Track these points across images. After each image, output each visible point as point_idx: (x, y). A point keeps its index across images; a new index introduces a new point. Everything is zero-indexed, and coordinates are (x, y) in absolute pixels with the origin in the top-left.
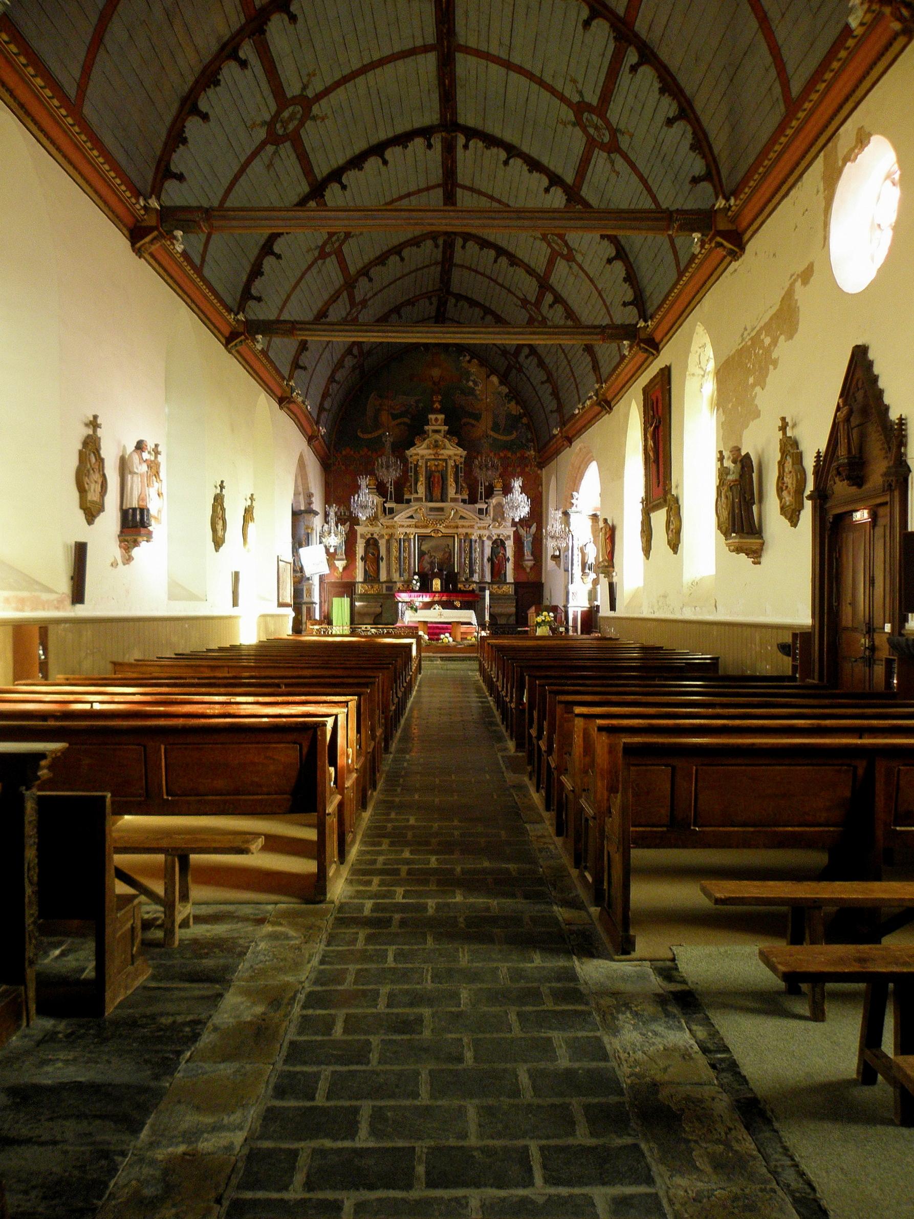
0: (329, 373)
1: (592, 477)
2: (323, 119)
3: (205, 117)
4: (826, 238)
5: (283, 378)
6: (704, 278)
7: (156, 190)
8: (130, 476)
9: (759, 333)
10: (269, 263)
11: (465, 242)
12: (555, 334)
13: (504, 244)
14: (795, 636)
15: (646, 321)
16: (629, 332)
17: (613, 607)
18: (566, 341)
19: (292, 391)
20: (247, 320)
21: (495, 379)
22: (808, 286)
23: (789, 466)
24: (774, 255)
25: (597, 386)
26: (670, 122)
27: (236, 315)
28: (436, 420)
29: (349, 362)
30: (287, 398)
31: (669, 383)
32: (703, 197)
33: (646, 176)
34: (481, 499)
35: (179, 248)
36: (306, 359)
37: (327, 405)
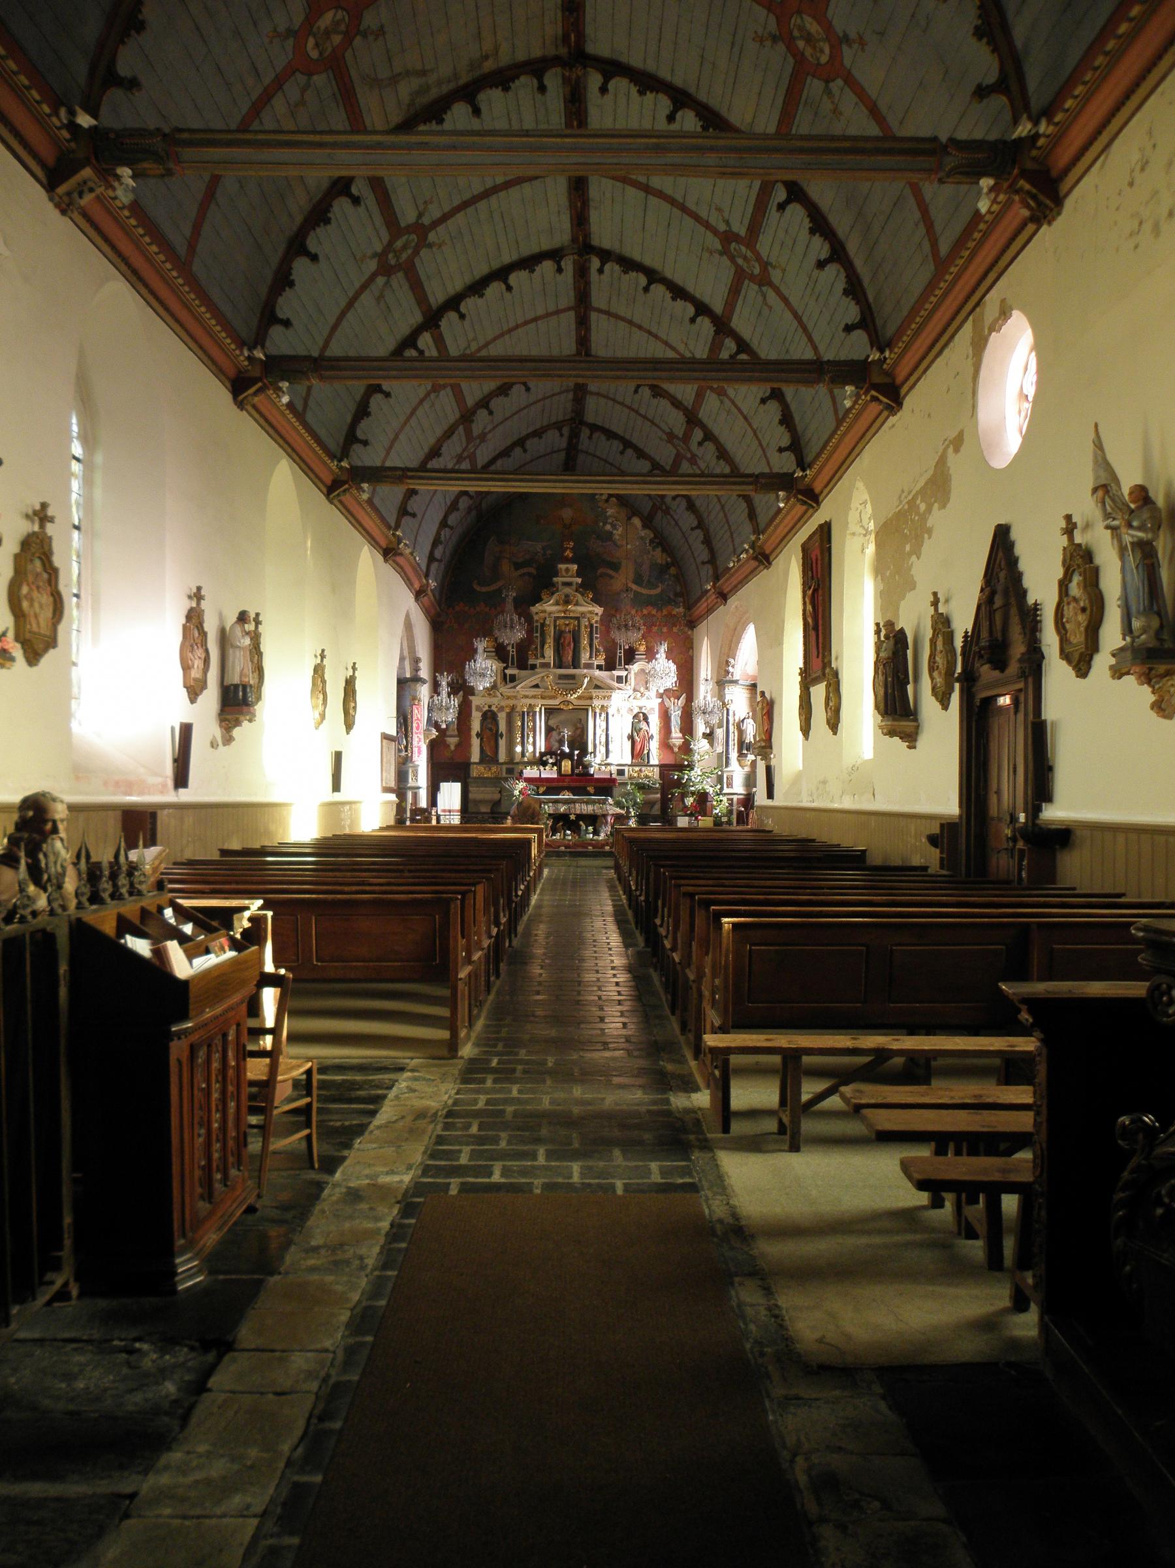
1: (749, 641)
2: (440, 246)
3: (314, 258)
4: (974, 407)
5: (389, 527)
6: (863, 430)
8: (231, 651)
9: (914, 498)
12: (704, 483)
14: (942, 825)
15: (804, 470)
16: (785, 482)
17: (770, 795)
19: (399, 541)
20: (352, 467)
21: (636, 521)
22: (959, 455)
23: (940, 646)
24: (1117, 209)
25: (753, 538)
26: (821, 265)
27: (340, 460)
28: (567, 570)
29: (464, 503)
31: (829, 541)
33: (800, 313)
34: (620, 664)
35: (285, 399)
37: (438, 554)
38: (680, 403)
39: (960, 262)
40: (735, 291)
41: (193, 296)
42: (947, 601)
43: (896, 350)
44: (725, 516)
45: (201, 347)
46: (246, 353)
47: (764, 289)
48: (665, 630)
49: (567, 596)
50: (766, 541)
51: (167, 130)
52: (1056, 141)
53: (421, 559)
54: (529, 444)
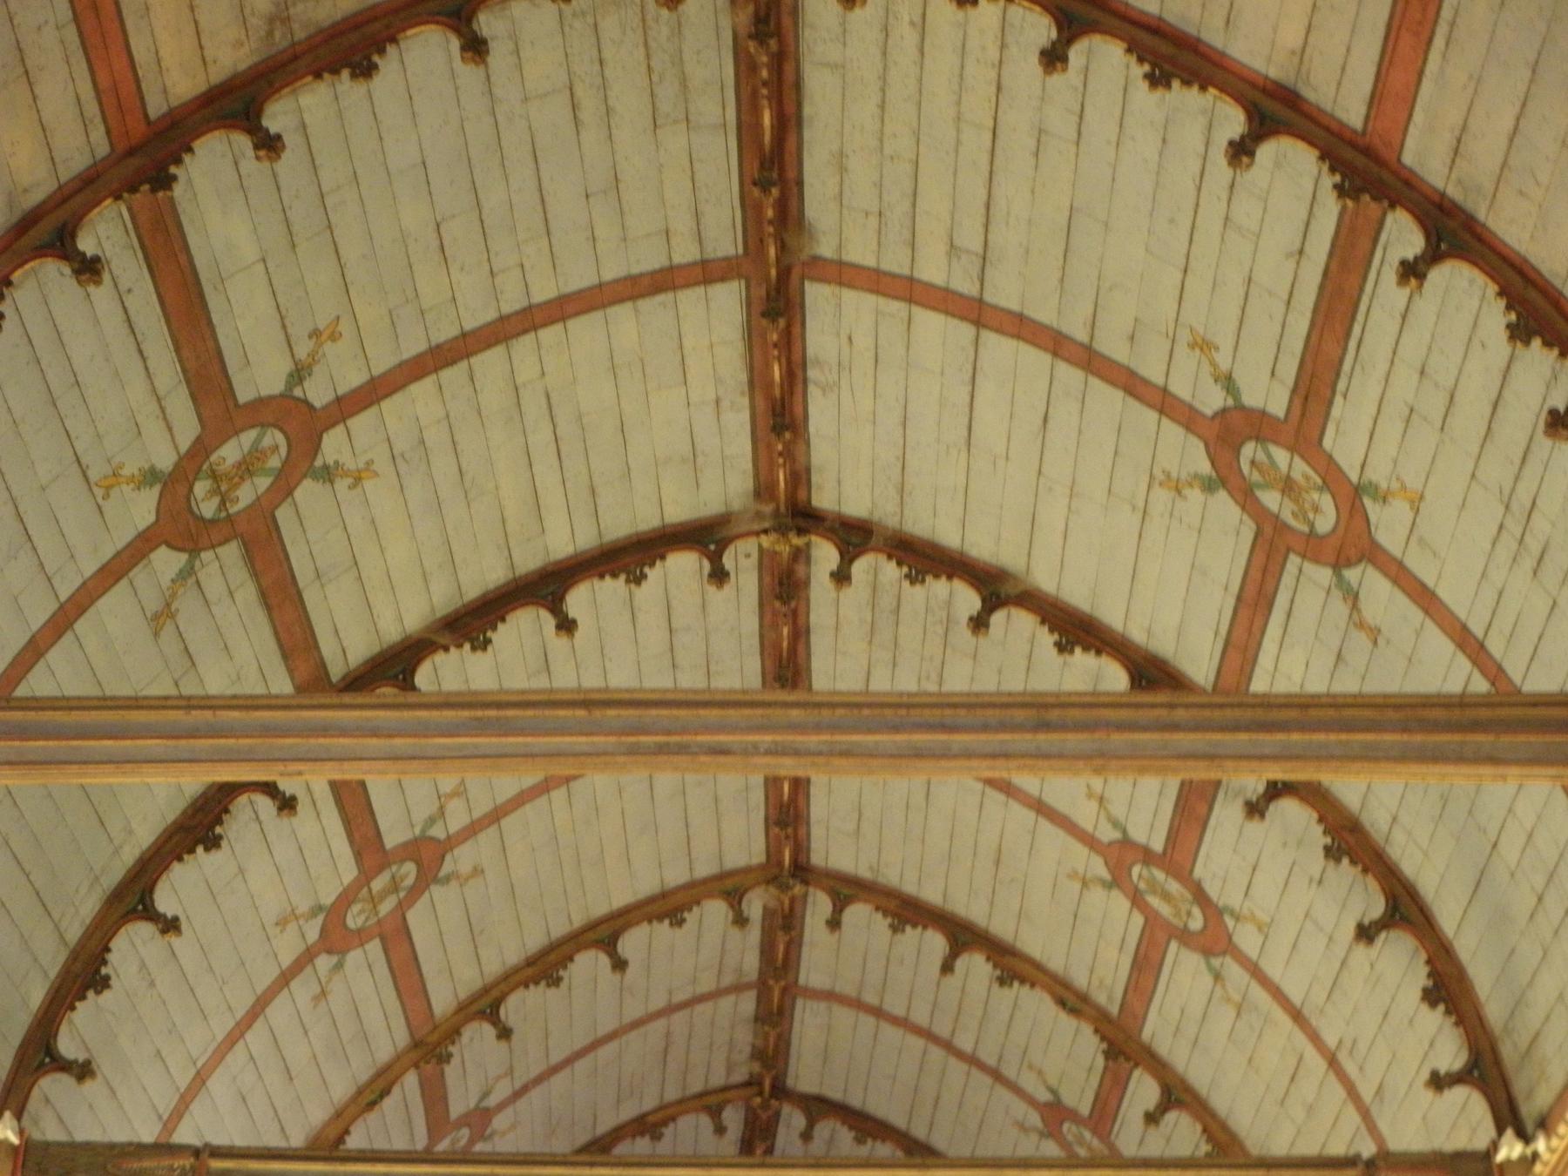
2: (358, 480)
10: (133, 946)
11: (840, 904)
13: (972, 909)
15: (1525, 1137)
33: (1477, 629)
38: (1084, 998)
47: (1352, 575)
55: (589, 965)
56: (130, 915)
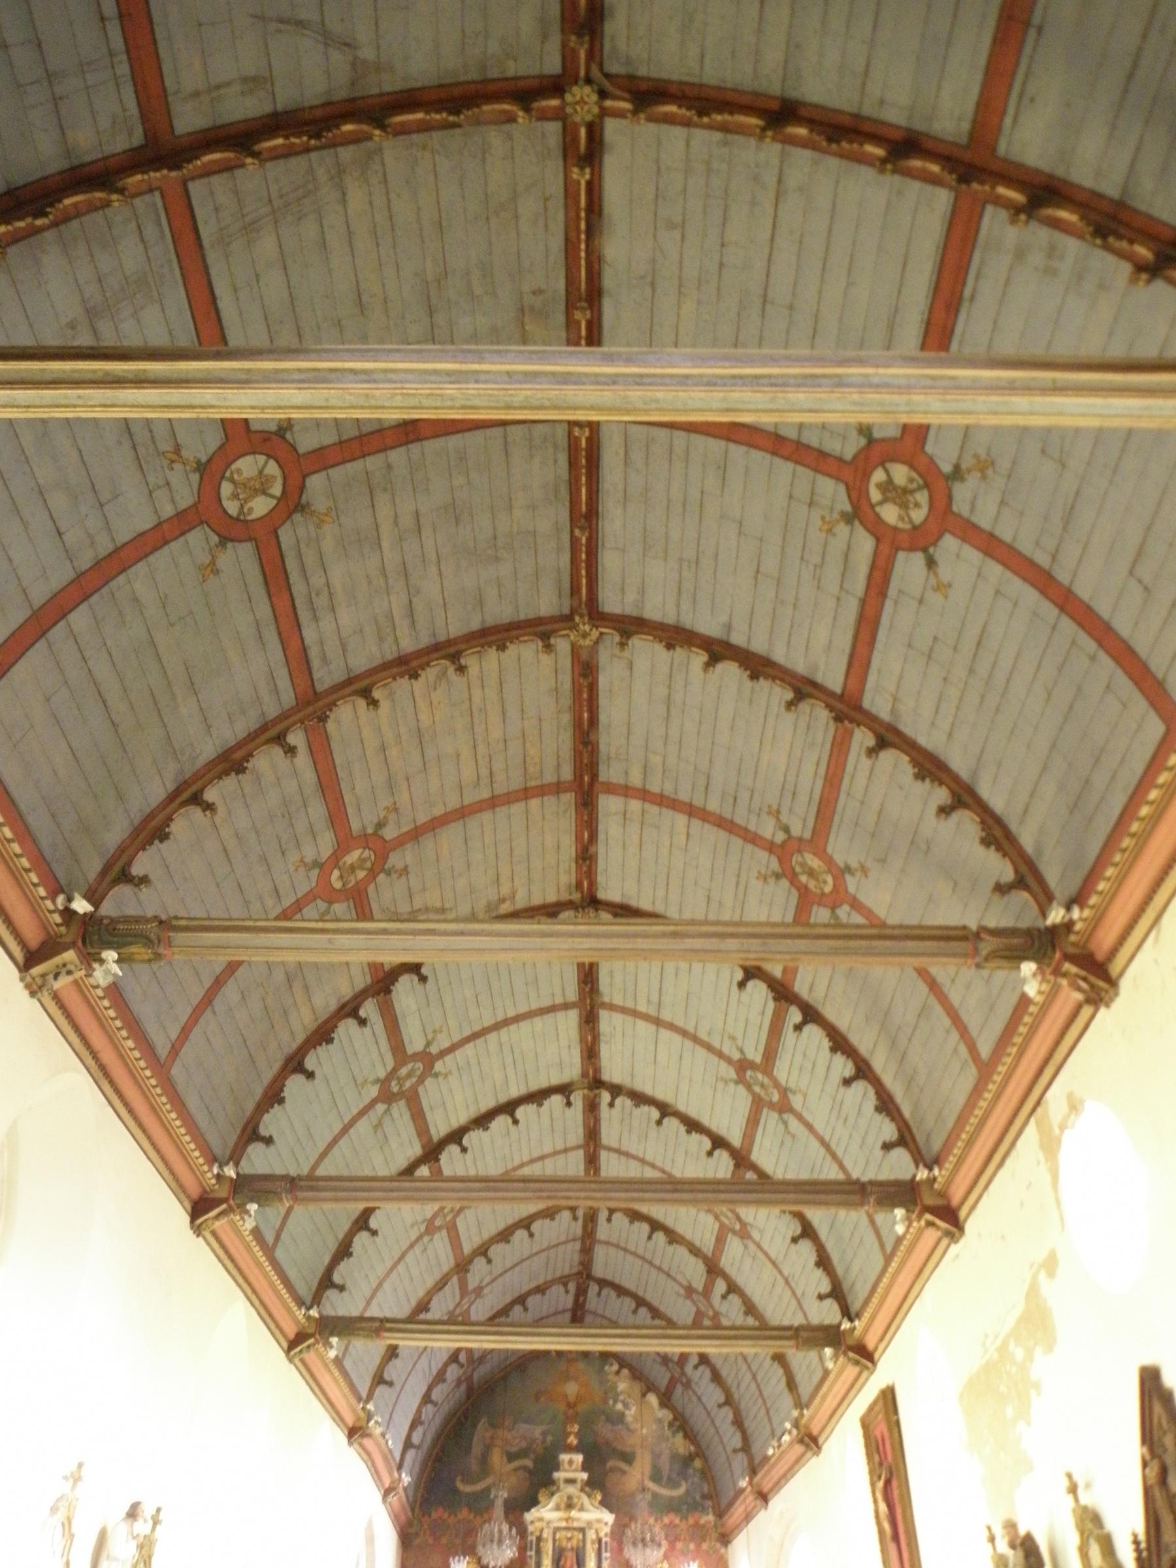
0: (424, 1389)
2: (446, 1076)
5: (359, 1399)
7: (235, 1157)
9: (1005, 1344)
10: (361, 1240)
12: (735, 1338)
15: (851, 1320)
16: (831, 1336)
18: (748, 1349)
19: (369, 1417)
21: (652, 1399)
24: (1003, 1237)
25: (795, 1413)
26: (847, 1082)
27: (308, 1309)
28: (571, 1462)
29: (453, 1372)
30: (360, 1428)
32: (900, 1165)
33: (827, 1138)
36: (393, 1372)
37: (416, 1438)
39: (1008, 1060)
40: (753, 1122)
41: (164, 1099)
42: (1088, 1486)
43: (947, 1165)
44: (758, 1386)
45: (163, 1158)
46: (215, 1171)
47: (785, 1116)
48: (692, 1546)
49: (570, 1498)
50: (814, 1417)
51: (164, 917)
52: (1096, 922)
53: (394, 1444)
54: (531, 1301)
55: (521, 1234)
56: (360, 1229)
